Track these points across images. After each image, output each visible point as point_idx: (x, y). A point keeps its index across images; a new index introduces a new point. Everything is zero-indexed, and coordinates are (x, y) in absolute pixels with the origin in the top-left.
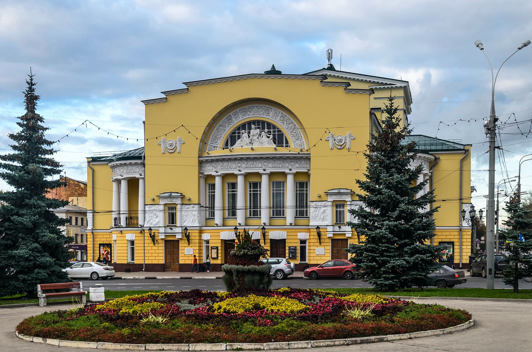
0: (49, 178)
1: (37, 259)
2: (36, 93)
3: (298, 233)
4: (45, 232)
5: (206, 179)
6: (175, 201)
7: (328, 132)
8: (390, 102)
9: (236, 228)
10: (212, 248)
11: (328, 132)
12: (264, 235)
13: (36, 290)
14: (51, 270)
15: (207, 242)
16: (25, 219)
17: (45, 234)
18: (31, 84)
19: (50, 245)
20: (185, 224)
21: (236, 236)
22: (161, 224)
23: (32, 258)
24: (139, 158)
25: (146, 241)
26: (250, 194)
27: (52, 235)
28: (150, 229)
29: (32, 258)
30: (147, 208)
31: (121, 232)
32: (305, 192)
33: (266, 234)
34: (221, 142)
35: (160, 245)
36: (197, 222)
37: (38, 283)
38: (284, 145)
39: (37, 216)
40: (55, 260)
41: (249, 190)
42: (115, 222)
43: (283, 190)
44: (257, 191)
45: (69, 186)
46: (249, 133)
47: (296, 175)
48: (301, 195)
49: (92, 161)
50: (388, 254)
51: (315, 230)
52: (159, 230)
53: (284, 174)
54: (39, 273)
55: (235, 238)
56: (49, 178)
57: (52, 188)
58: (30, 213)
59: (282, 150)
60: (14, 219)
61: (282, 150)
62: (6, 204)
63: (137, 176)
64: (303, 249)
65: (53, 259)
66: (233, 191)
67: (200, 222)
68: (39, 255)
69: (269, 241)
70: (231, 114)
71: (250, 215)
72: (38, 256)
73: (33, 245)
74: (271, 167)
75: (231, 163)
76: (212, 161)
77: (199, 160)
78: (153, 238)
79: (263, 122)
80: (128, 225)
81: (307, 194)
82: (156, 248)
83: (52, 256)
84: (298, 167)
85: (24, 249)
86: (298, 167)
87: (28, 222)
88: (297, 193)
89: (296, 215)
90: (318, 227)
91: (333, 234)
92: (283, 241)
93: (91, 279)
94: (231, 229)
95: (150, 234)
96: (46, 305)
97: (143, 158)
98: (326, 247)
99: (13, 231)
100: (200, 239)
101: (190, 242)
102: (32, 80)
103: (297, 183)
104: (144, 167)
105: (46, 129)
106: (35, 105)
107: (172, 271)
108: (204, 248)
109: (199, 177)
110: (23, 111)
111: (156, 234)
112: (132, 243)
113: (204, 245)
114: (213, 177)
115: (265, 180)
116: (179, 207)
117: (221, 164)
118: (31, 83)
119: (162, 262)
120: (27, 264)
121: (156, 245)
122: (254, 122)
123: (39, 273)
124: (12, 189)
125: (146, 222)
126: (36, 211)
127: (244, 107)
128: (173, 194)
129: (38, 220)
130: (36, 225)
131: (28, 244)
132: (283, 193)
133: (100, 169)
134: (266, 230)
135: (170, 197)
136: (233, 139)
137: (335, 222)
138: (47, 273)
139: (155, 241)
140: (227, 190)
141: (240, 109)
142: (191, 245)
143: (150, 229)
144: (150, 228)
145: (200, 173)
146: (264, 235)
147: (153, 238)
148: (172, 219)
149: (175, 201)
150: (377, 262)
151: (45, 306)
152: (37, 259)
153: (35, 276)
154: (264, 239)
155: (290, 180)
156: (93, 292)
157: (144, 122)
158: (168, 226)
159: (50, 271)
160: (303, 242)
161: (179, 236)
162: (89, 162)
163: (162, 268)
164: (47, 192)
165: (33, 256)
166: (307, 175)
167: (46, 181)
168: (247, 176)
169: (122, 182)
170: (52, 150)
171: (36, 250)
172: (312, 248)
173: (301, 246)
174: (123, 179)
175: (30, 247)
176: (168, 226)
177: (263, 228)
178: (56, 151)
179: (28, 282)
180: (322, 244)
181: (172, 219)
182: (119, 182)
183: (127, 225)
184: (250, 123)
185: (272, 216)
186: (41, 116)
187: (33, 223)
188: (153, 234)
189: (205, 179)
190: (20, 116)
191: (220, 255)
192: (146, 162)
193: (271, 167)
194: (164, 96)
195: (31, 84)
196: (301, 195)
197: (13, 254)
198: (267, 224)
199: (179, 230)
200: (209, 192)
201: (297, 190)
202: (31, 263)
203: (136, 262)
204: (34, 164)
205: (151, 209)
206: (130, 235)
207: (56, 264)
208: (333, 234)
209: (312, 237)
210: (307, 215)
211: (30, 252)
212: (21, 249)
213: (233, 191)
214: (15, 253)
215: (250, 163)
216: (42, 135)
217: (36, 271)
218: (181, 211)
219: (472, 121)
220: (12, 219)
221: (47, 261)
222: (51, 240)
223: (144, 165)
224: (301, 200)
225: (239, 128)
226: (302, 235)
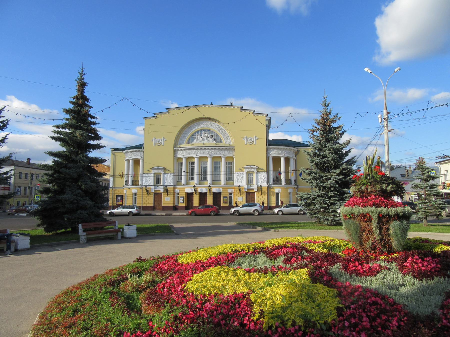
0: (92, 142)
1: (80, 202)
2: (85, 81)
4: (87, 182)
6: (160, 171)
7: (291, 115)
8: (324, 99)
9: (194, 186)
10: (180, 197)
11: (291, 115)
13: (78, 227)
14: (91, 211)
16: (71, 171)
17: (87, 182)
18: (82, 74)
19: (91, 191)
20: (166, 184)
21: (194, 191)
22: (152, 184)
23: (76, 201)
24: (141, 148)
25: (143, 194)
27: (93, 184)
28: (146, 187)
29: (76, 201)
30: (144, 175)
31: (129, 188)
32: (231, 167)
33: (211, 189)
34: (186, 140)
35: (151, 195)
37: (80, 222)
39: (81, 169)
40: (94, 203)
42: (126, 183)
43: (220, 166)
45: (99, 167)
48: (229, 169)
49: (114, 151)
50: (335, 199)
51: (238, 187)
53: (220, 157)
54: (80, 213)
55: (193, 191)
56: (92, 142)
57: (93, 149)
58: (76, 166)
60: (62, 171)
62: (56, 159)
63: (139, 158)
64: (231, 198)
65: (93, 202)
66: (192, 166)
67: (173, 183)
68: (81, 199)
70: (191, 125)
71: (202, 179)
72: (80, 200)
73: (77, 191)
74: (214, 153)
76: (181, 150)
77: (174, 149)
78: (147, 191)
80: (133, 185)
82: (149, 197)
83: (92, 199)
84: (227, 154)
85: (70, 194)
86: (227, 154)
87: (74, 173)
88: (227, 168)
90: (239, 186)
92: (220, 194)
95: (146, 190)
96: (86, 242)
98: (243, 197)
99: (62, 181)
100: (174, 192)
101: (168, 194)
102: (83, 71)
103: (227, 162)
104: (143, 153)
105: (91, 107)
106: (84, 89)
107: (158, 210)
109: (174, 159)
110: (75, 93)
111: (149, 190)
112: (135, 194)
114: (181, 158)
116: (162, 175)
118: (82, 73)
119: (152, 205)
120: (71, 206)
121: (149, 195)
123: (80, 213)
124: (64, 149)
125: (144, 183)
126: (80, 165)
127: (198, 122)
128: (159, 168)
129: (82, 172)
130: (80, 176)
131: (73, 191)
132: (220, 168)
133: (118, 154)
134: (196, 187)
135: (158, 169)
138: (87, 214)
140: (189, 166)
141: (196, 123)
142: (169, 195)
143: (146, 187)
144: (146, 186)
145: (174, 157)
146: (195, 191)
147: (147, 191)
148: (158, 181)
149: (160, 171)
150: (326, 204)
151: (85, 243)
152: (80, 202)
153: (77, 216)
154: (210, 192)
156: (127, 229)
157: (144, 129)
159: (90, 212)
160: (231, 194)
161: (162, 191)
162: (112, 151)
163: (153, 208)
164: (90, 151)
165: (77, 200)
166: (232, 158)
167: (90, 144)
169: (131, 161)
170: (96, 122)
171: (79, 195)
172: (235, 197)
173: (229, 196)
174: (131, 159)
175: (74, 193)
177: (210, 186)
178: (98, 124)
179: (72, 221)
180: (241, 195)
181: (158, 181)
182: (128, 161)
183: (132, 184)
186: (87, 98)
187: (78, 174)
188: (147, 190)
189: (177, 160)
190: (73, 97)
191: (185, 201)
192: (144, 150)
193: (214, 153)
194: (166, 111)
195: (82, 74)
196: (229, 169)
197: (60, 198)
199: (162, 187)
200: (179, 167)
201: (227, 166)
202: (74, 205)
204: (81, 131)
205: (147, 176)
206: (134, 190)
207: (94, 206)
209: (235, 191)
210: (232, 179)
211: (75, 197)
212: (67, 194)
213: (192, 166)
214: (61, 197)
215: (202, 151)
216: (88, 111)
217: (79, 211)
218: (164, 176)
219: (374, 114)
220: (61, 171)
221: (88, 204)
222: (91, 188)
223: (143, 152)
224: (229, 171)
225: (195, 133)
226: (230, 191)
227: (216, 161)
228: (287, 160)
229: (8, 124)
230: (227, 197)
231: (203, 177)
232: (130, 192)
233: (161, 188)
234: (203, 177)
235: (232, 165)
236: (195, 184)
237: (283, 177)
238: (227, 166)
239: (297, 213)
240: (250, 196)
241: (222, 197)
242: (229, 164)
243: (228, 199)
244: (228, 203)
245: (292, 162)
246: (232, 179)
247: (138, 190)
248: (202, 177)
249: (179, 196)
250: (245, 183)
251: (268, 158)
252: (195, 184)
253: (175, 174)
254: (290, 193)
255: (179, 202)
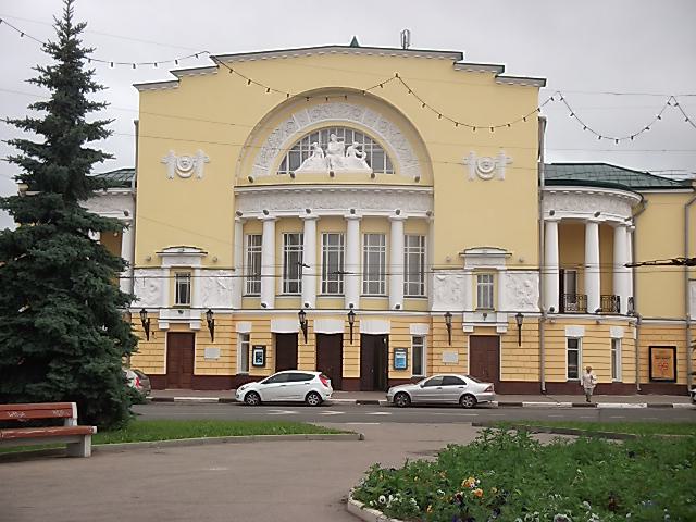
3: (411, 325)
5: (244, 225)
6: (491, 263)
12: (304, 327)
15: (246, 337)
24: (128, 184)
26: (324, 253)
28: (143, 312)
32: (339, 251)
36: (230, 300)
38: (385, 170)
41: (322, 246)
44: (337, 248)
46: (325, 148)
47: (408, 221)
52: (158, 313)
59: (382, 178)
61: (382, 178)
64: (418, 352)
66: (257, 249)
69: (314, 336)
71: (324, 291)
75: (580, 202)
79: (349, 131)
81: (342, 254)
89: (405, 293)
90: (448, 315)
91: (170, 324)
93: (305, 404)
94: (343, 315)
97: (133, 184)
98: (461, 351)
108: (239, 348)
113: (240, 342)
115: (354, 230)
117: (274, 198)
122: (333, 130)
128: (187, 250)
134: (306, 318)
135: (181, 254)
136: (295, 157)
137: (476, 307)
139: (150, 334)
146: (304, 327)
148: (183, 295)
155: (398, 232)
157: (136, 123)
158: (175, 307)
160: (418, 339)
166: (426, 222)
168: (279, 221)
176: (175, 307)
181: (183, 295)
184: (324, 131)
185: (321, 293)
198: (311, 305)
200: (249, 250)
203: (619, 379)
208: (170, 324)
213: (257, 249)
224: (374, 265)
226: (419, 329)
227: (377, 229)
228: (608, 231)
229: (94, 91)
230: (406, 350)
231: (334, 277)
232: (605, 334)
233: (194, 319)
234: (334, 277)
235: (342, 243)
236: (303, 307)
237: (593, 286)
238: (408, 247)
239: (303, 400)
240: (485, 354)
241: (391, 350)
242: (418, 239)
243: (411, 357)
244: (411, 368)
245: (623, 240)
246: (383, 292)
247: (589, 328)
248: (324, 284)
249: (252, 343)
250: (472, 305)
251: (543, 226)
252: (303, 307)
253: (238, 272)
254: (614, 341)
255: (250, 365)
